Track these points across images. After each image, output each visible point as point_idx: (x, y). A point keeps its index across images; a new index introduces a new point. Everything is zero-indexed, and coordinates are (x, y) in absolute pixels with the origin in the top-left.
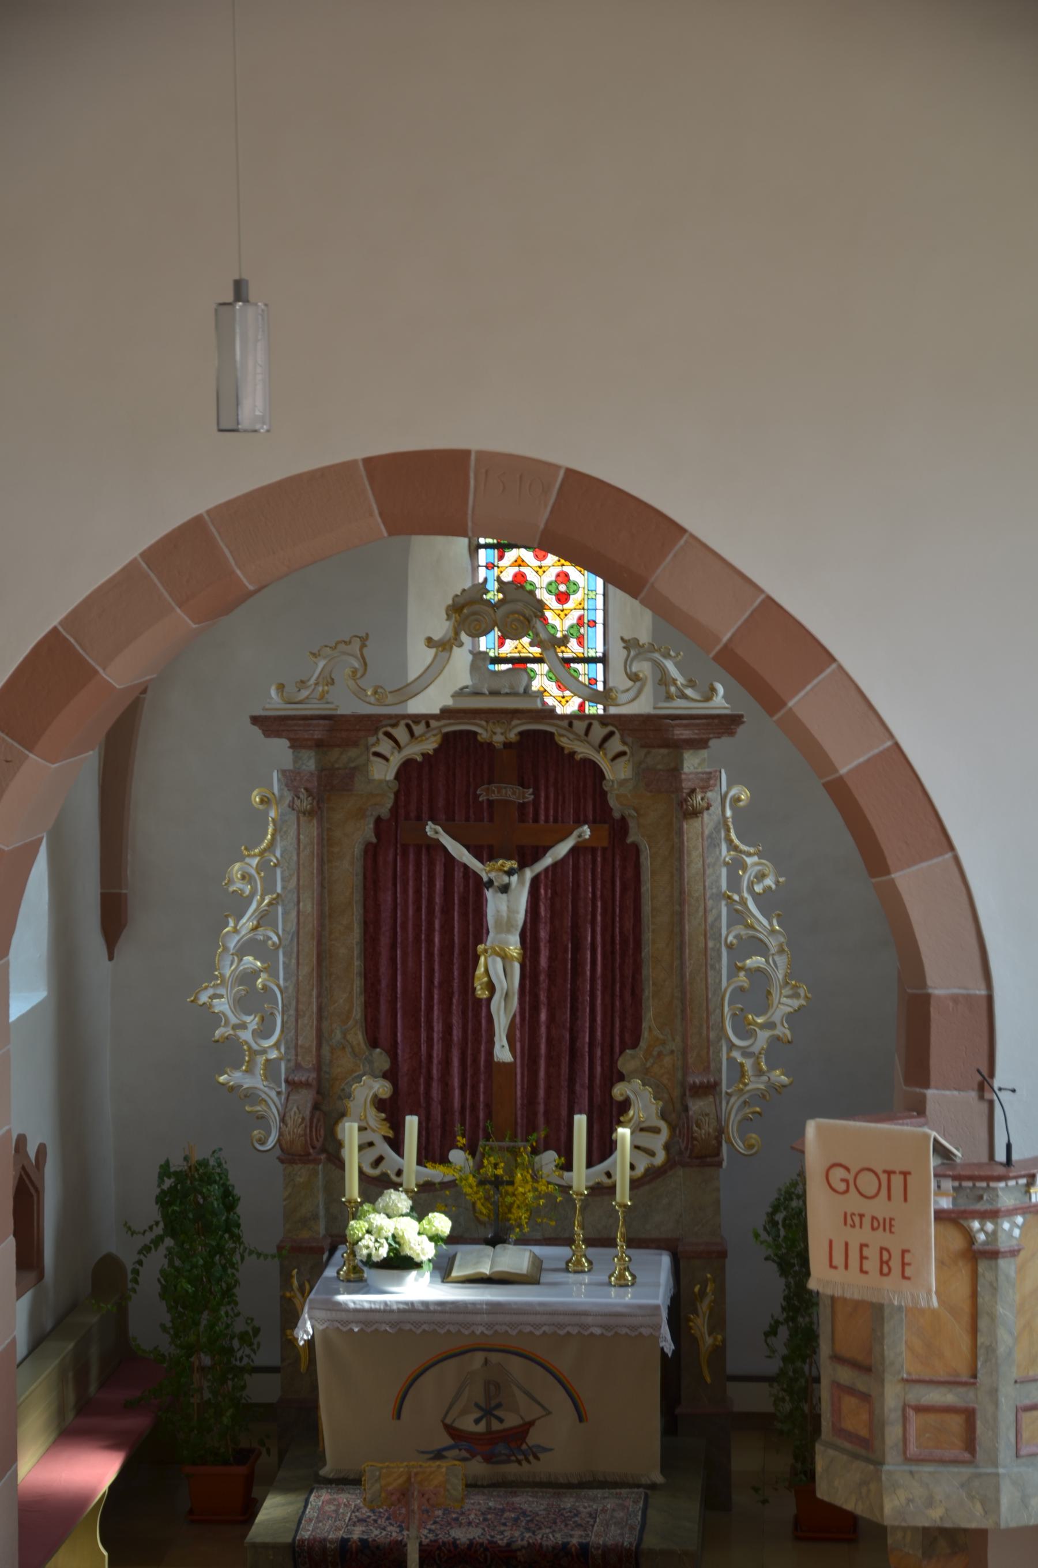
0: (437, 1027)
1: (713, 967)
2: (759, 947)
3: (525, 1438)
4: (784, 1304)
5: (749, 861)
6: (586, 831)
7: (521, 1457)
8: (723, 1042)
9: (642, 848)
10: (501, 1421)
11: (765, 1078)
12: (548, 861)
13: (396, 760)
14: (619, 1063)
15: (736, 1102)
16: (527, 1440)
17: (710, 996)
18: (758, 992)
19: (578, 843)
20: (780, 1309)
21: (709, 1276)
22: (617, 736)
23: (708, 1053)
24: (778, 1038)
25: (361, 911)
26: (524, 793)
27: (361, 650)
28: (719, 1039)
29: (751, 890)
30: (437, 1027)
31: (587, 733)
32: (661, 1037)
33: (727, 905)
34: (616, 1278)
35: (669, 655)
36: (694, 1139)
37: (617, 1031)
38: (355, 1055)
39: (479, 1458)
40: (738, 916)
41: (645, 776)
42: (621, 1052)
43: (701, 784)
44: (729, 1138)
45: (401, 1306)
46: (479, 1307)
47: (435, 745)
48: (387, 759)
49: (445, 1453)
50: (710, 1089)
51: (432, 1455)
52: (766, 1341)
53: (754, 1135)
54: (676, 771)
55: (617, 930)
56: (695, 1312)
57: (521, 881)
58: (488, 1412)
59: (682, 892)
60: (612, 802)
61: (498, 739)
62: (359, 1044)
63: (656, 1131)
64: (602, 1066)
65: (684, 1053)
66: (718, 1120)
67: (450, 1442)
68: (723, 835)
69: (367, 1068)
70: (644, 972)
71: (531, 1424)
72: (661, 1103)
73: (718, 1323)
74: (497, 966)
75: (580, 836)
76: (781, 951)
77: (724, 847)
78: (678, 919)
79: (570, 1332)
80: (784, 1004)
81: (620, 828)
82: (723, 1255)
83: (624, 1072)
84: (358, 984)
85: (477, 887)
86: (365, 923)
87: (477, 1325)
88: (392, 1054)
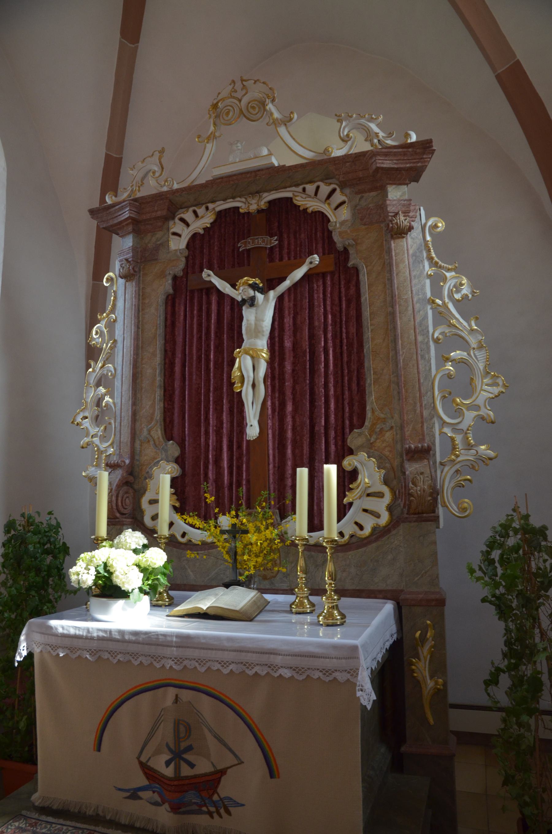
0: (212, 421)
1: (423, 357)
2: (460, 342)
3: (217, 787)
4: (505, 649)
5: (448, 275)
6: (316, 258)
7: (212, 809)
8: (435, 419)
9: (360, 268)
10: (192, 765)
11: (473, 452)
12: (287, 284)
13: (186, 234)
14: (349, 440)
15: (449, 471)
16: (219, 790)
17: (422, 381)
18: (462, 383)
19: (310, 269)
20: (500, 656)
21: (429, 622)
22: (338, 190)
23: (422, 426)
24: (483, 418)
25: (163, 342)
26: (271, 240)
27: (160, 159)
28: (432, 417)
29: (451, 297)
30: (212, 421)
31: (316, 194)
32: (382, 416)
33: (432, 308)
34: (325, 617)
35: (372, 118)
36: (411, 495)
37: (347, 415)
38: (155, 445)
39: (166, 806)
40: (442, 316)
41: (362, 217)
42: (351, 431)
43: (403, 209)
44: (444, 502)
45: (101, 634)
46: (169, 639)
47: (212, 221)
48: (180, 236)
49: (140, 794)
50: (424, 453)
51: (128, 794)
52: (486, 690)
53: (466, 500)
54: (382, 207)
55: (344, 335)
56: (417, 656)
57: (266, 299)
58: (178, 756)
59: (393, 296)
60: (336, 238)
61: (253, 208)
62: (159, 438)
63: (380, 495)
64: (336, 445)
65: (402, 428)
66: (433, 479)
67: (144, 782)
68: (425, 255)
69: (164, 456)
70: (366, 365)
71: (223, 772)
72: (383, 471)
73: (439, 666)
74: (248, 361)
75: (311, 263)
76: (480, 347)
77: (426, 264)
78: (391, 317)
79: (257, 671)
80: (485, 391)
81: (344, 255)
82: (441, 603)
83: (353, 448)
84: (159, 393)
85: (237, 308)
86: (166, 351)
87: (168, 658)
88: (182, 445)
